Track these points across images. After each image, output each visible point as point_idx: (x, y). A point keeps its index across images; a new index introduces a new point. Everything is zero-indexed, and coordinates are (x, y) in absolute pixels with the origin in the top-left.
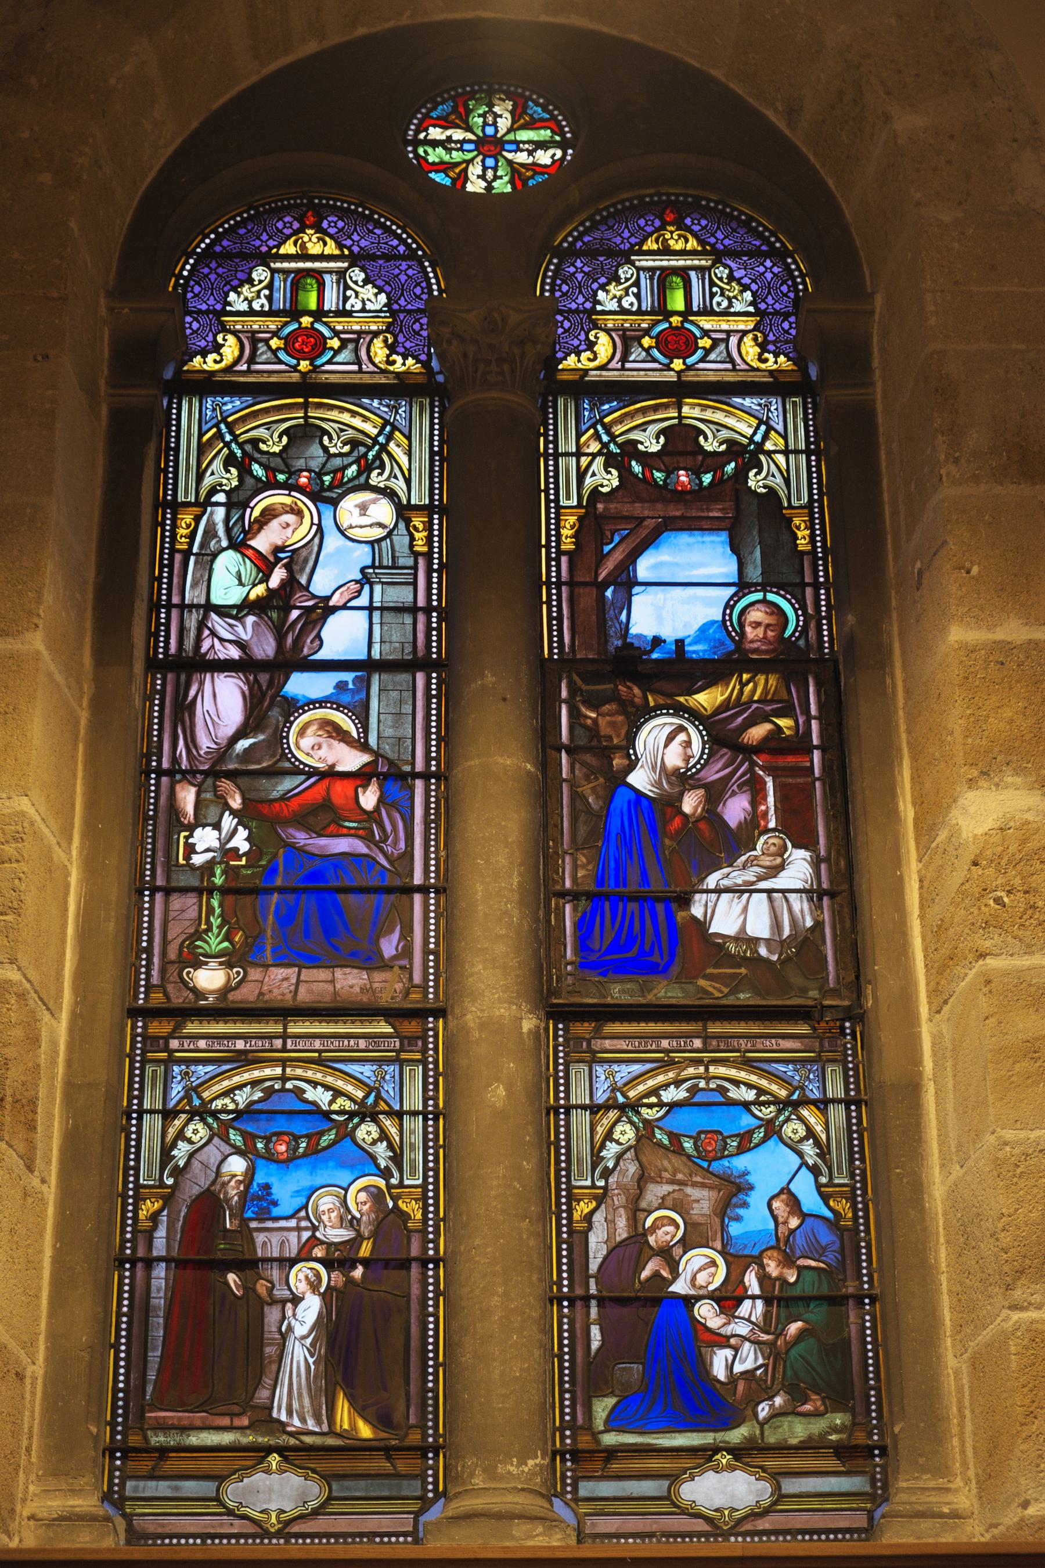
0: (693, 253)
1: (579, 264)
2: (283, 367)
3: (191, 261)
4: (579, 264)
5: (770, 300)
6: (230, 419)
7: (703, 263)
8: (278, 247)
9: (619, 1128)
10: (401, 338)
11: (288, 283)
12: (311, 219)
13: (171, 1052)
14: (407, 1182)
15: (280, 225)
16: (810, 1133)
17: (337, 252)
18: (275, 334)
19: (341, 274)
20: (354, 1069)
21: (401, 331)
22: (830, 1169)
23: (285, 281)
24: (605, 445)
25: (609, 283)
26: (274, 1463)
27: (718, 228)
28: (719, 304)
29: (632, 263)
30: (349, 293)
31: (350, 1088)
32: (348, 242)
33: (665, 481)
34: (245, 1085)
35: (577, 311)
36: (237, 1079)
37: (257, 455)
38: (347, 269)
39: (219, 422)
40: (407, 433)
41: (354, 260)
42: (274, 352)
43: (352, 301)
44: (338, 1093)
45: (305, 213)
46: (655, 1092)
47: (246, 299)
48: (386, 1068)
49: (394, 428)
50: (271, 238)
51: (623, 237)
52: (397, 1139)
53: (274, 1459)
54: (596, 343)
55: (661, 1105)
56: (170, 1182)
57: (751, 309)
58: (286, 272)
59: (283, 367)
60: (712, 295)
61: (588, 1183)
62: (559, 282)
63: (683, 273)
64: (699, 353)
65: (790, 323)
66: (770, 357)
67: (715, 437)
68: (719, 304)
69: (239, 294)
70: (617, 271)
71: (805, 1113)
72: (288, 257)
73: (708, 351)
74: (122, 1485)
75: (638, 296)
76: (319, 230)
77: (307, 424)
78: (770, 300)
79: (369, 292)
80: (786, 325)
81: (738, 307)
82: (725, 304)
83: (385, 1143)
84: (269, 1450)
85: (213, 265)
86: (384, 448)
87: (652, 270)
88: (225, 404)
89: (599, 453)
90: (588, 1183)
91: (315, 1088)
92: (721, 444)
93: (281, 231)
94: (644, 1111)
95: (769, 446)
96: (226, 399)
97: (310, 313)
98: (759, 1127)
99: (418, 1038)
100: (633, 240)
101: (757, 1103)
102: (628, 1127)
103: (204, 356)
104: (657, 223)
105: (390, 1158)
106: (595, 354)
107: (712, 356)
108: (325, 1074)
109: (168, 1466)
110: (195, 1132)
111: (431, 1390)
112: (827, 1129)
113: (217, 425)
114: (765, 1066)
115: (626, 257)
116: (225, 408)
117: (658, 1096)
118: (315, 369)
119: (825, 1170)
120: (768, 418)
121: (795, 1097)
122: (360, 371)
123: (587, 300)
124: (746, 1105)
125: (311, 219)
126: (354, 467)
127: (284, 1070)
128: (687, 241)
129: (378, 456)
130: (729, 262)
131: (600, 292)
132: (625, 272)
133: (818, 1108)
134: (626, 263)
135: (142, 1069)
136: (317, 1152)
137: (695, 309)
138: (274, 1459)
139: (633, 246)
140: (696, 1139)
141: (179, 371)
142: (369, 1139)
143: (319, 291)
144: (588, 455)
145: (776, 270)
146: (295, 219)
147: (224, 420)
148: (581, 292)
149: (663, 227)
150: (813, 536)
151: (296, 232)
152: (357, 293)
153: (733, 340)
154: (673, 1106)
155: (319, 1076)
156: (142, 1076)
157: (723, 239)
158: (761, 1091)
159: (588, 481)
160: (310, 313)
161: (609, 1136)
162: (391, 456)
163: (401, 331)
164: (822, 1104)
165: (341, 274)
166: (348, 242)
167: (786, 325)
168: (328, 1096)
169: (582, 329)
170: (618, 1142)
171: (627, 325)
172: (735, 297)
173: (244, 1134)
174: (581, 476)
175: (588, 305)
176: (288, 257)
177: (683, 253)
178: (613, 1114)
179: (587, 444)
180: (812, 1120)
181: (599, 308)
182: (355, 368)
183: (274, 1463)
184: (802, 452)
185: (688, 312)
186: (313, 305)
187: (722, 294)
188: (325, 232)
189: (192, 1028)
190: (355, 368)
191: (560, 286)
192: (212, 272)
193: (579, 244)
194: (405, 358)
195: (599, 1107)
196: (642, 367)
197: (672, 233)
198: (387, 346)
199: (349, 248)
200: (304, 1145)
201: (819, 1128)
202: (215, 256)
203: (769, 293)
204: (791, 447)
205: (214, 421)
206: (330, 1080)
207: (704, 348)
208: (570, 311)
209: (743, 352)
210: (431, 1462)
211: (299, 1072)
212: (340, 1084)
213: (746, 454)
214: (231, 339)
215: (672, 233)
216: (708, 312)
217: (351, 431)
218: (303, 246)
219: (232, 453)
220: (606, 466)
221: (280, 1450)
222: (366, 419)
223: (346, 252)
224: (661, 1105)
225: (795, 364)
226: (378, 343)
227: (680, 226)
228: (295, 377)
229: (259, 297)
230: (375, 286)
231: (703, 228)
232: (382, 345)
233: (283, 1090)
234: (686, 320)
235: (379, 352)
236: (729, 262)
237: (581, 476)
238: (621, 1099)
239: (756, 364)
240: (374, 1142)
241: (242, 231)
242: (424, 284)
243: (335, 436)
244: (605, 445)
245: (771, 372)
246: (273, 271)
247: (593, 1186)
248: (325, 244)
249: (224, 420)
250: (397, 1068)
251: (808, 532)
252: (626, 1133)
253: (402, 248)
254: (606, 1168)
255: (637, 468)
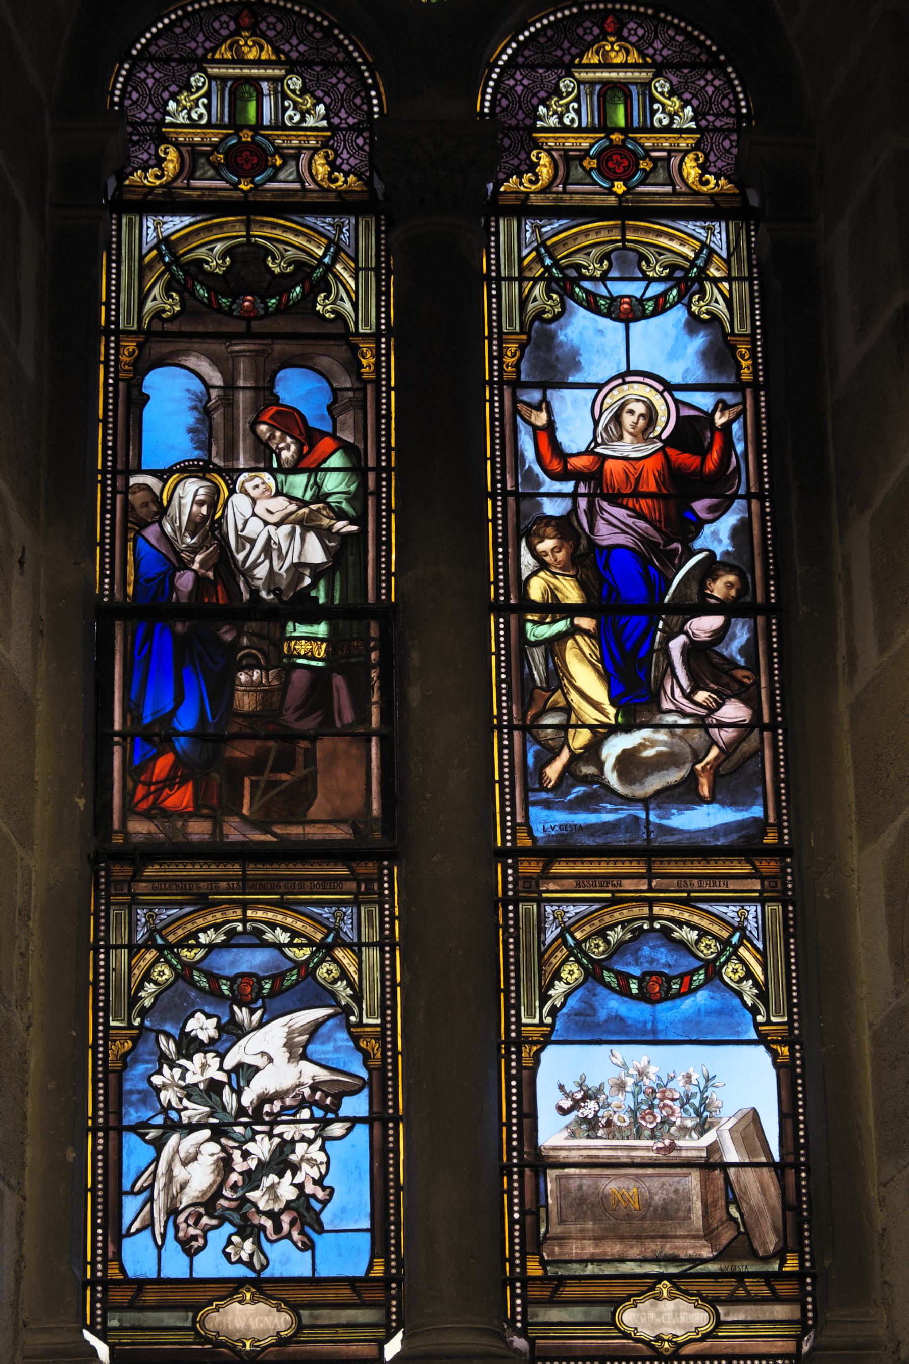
0: (268, 63)
1: (518, 76)
2: (597, 188)
3: (127, 66)
4: (150, 69)
5: (343, 114)
6: (549, 243)
7: (277, 72)
8: (581, 56)
9: (567, 968)
10: (712, 158)
11: (595, 98)
12: (246, 21)
13: (134, 895)
14: (365, 1021)
15: (580, 31)
16: (344, 974)
17: (273, 57)
18: (215, 147)
19: (646, 86)
20: (719, 909)
21: (711, 149)
22: (361, 1010)
23: (592, 94)
24: (548, 269)
25: (180, 93)
26: (665, 1291)
27: (656, 37)
28: (291, 118)
29: (205, 72)
30: (656, 106)
31: (715, 929)
32: (287, 48)
33: (230, 307)
34: (616, 925)
35: (516, 128)
36: (200, 922)
37: (201, 278)
38: (285, 77)
39: (539, 245)
40: (352, 254)
41: (292, 67)
42: (588, 172)
43: (659, 115)
44: (704, 933)
45: (241, 12)
46: (194, 935)
47: (555, 112)
48: (747, 908)
49: (712, 251)
50: (207, 39)
51: (198, 44)
52: (356, 977)
53: (664, 1287)
54: (538, 164)
55: (200, 945)
56: (137, 1022)
57: (324, 123)
58: (223, 79)
59: (597, 188)
60: (285, 109)
61: (537, 1021)
62: (129, 89)
63: (622, 88)
64: (269, 172)
65: (365, 139)
66: (711, 178)
67: (657, 261)
68: (291, 118)
69: (548, 107)
70: (557, 84)
71: (339, 953)
72: (223, 61)
73: (278, 169)
74: (104, 1317)
75: (578, 112)
76: (620, 38)
77: (249, 243)
78: (343, 114)
79: (674, 103)
80: (360, 141)
81: (310, 122)
82: (297, 118)
83: (751, 982)
84: (660, 1277)
85: (341, 74)
86: (330, 268)
87: (592, 83)
88: (544, 226)
89: (541, 278)
90: (537, 1021)
91: (681, 928)
92: (289, 265)
93: (217, 32)
94: (185, 952)
95: (713, 272)
96: (166, 219)
97: (250, 128)
98: (291, 970)
99: (374, 880)
100: (208, 45)
101: (290, 945)
102: (575, 968)
103: (145, 170)
104: (596, 31)
105: (351, 996)
106: (536, 175)
107: (282, 176)
108: (692, 914)
109: (569, 1292)
110: (161, 973)
111: (99, 1226)
112: (360, 971)
113: (536, 249)
114: (705, 906)
115: (200, 63)
116: (544, 230)
117: (197, 938)
118: (256, 188)
119: (762, 1009)
120: (339, 238)
121: (330, 940)
122: (674, 193)
123: (527, 116)
124: (279, 946)
125: (246, 21)
126: (675, 292)
127: (651, 910)
128: (261, 48)
129: (324, 277)
130: (670, 76)
131: (541, 108)
132: (197, 79)
133: (353, 951)
134: (198, 71)
135: (107, 912)
136: (281, 992)
137: (635, 125)
138: (664, 1287)
139: (207, 51)
140: (641, 980)
141: (120, 187)
142: (737, 977)
143: (257, 100)
144: (529, 279)
145: (717, 83)
146: (595, 24)
147: (543, 244)
148: (520, 107)
149: (237, 33)
150: (378, 365)
151: (597, 40)
152: (295, 103)
153: (304, 158)
154: (211, 947)
155: (686, 916)
156: (107, 917)
157: (296, 48)
158: (295, 933)
159: (149, 304)
160: (250, 128)
161: (147, 977)
162: (337, 278)
163: (711, 149)
164: (356, 947)
165: (646, 86)
166: (287, 48)
167: (727, 144)
168: (694, 935)
169: (523, 147)
170: (156, 983)
171: (197, 139)
172: (676, 113)
173: (618, 974)
174: (523, 303)
175: (528, 122)
176: (223, 61)
177: (625, 65)
178: (150, 956)
179: (529, 267)
180: (346, 962)
181: (539, 124)
182: (669, 189)
183: (665, 1291)
184: (505, 279)
185: (628, 129)
186: (622, 123)
187: (663, 112)
188: (263, 35)
189: (559, 869)
190: (669, 189)
191: (130, 93)
192: (150, 76)
193: (153, 49)
194: (346, 175)
195: (140, 947)
196: (587, 190)
197: (612, 44)
198: (329, 163)
199: (652, 57)
200: (268, 986)
201: (352, 970)
202: (152, 59)
203: (342, 106)
204: (735, 274)
205: (535, 244)
206: (696, 919)
207: (644, 170)
208: (510, 128)
209: (685, 174)
210: (393, 1292)
211: (260, 914)
212: (705, 923)
213: (314, 277)
214: (172, 150)
215: (612, 44)
216: (643, 130)
217: (669, 255)
218: (239, 50)
219: (173, 277)
220: (549, 291)
221: (669, 1277)
222: (683, 243)
223: (649, 60)
224: (200, 945)
225: (736, 186)
226: (319, 160)
227: (255, 31)
228: (612, 200)
229: (197, 106)
230: (680, 98)
231: (278, 33)
232: (323, 161)
233: (652, 929)
234: (256, 134)
235: (320, 169)
236: (670, 76)
237: (523, 303)
238: (160, 941)
239: (698, 187)
240: (740, 981)
241: (178, 30)
242: (731, 96)
243: (653, 260)
244: (548, 269)
245: (711, 196)
246: (211, 78)
247: (541, 1024)
248: (261, 48)
249: (543, 244)
250: (355, 910)
251: (373, 360)
252: (164, 973)
253: (704, 57)
254: (554, 1006)
255: (203, 292)
